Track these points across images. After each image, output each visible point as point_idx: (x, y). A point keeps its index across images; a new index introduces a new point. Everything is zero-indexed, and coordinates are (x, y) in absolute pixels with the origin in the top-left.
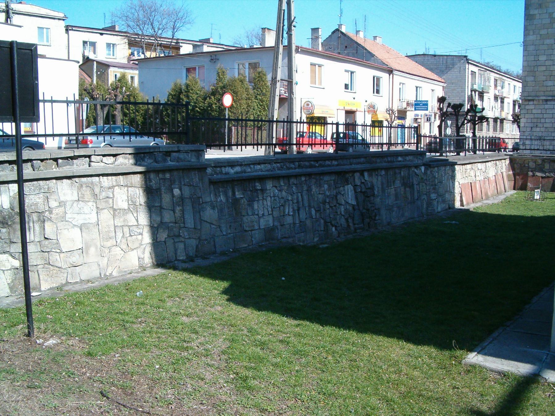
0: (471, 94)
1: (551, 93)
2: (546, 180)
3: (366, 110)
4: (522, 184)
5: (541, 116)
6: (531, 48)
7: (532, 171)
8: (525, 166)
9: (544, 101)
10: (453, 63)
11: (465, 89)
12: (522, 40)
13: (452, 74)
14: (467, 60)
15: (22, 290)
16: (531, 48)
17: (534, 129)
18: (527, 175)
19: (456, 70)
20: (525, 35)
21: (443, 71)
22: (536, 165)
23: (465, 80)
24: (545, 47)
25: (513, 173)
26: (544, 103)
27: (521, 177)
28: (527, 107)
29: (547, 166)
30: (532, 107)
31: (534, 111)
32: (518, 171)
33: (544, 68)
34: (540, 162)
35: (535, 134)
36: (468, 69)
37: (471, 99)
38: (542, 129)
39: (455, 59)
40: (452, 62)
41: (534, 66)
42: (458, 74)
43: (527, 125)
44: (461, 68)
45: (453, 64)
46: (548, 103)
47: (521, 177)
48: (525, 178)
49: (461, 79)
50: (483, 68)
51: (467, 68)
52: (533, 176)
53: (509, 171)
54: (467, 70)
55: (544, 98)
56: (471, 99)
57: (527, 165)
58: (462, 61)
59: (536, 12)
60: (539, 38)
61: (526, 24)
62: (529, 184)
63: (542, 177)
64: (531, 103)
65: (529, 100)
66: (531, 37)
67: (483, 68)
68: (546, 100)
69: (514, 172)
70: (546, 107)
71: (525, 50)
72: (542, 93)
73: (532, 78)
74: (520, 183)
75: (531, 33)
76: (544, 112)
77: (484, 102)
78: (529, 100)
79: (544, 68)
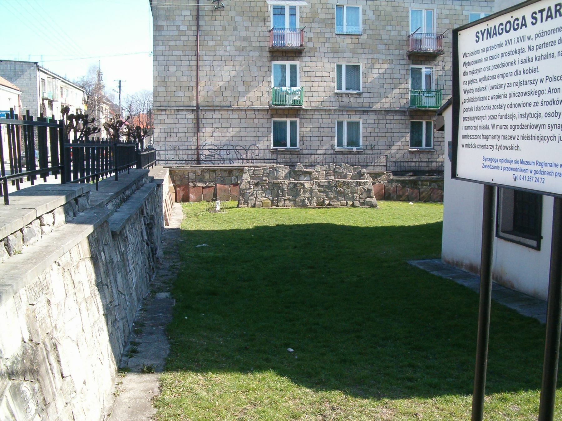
0: (43, 103)
1: (182, 104)
2: (207, 190)
3: (254, 113)
4: (183, 196)
5: (174, 126)
6: (161, 58)
7: (192, 182)
8: (184, 177)
9: (176, 111)
10: (22, 70)
11: (37, 97)
12: (151, 49)
13: (24, 80)
14: (38, 66)
15: (306, 394)
16: (161, 58)
17: (168, 139)
18: (187, 187)
19: (25, 77)
20: (154, 46)
21: (11, 78)
22: (196, 175)
23: (37, 88)
24: (174, 58)
25: (174, 185)
26: (177, 113)
27: (182, 188)
28: (160, 117)
29: (207, 176)
30: (164, 117)
31: (167, 121)
32: (178, 183)
33: (174, 79)
34: (199, 172)
35: (169, 144)
36: (39, 76)
37: (43, 107)
38: (176, 139)
39: (24, 66)
40: (21, 68)
41: (165, 76)
42: (29, 82)
43: (160, 135)
44: (32, 75)
45: (23, 71)
46: (180, 113)
47: (182, 188)
48: (186, 189)
49: (32, 87)
50: (51, 75)
51: (38, 75)
52: (194, 186)
53: (170, 183)
54: (38, 77)
55: (176, 108)
56: (43, 107)
57: (186, 176)
58: (32, 68)
59: (164, 23)
60: (168, 49)
61: (155, 35)
62: (191, 195)
63: (203, 188)
64: (164, 113)
65: (161, 110)
66: (161, 48)
67: (51, 75)
68: (178, 110)
69: (174, 184)
70: (179, 116)
71: (155, 60)
72: (173, 104)
73: (163, 89)
74: (181, 194)
75: (160, 43)
76: (176, 121)
77: (53, 111)
78: (161, 110)
79: (174, 79)
